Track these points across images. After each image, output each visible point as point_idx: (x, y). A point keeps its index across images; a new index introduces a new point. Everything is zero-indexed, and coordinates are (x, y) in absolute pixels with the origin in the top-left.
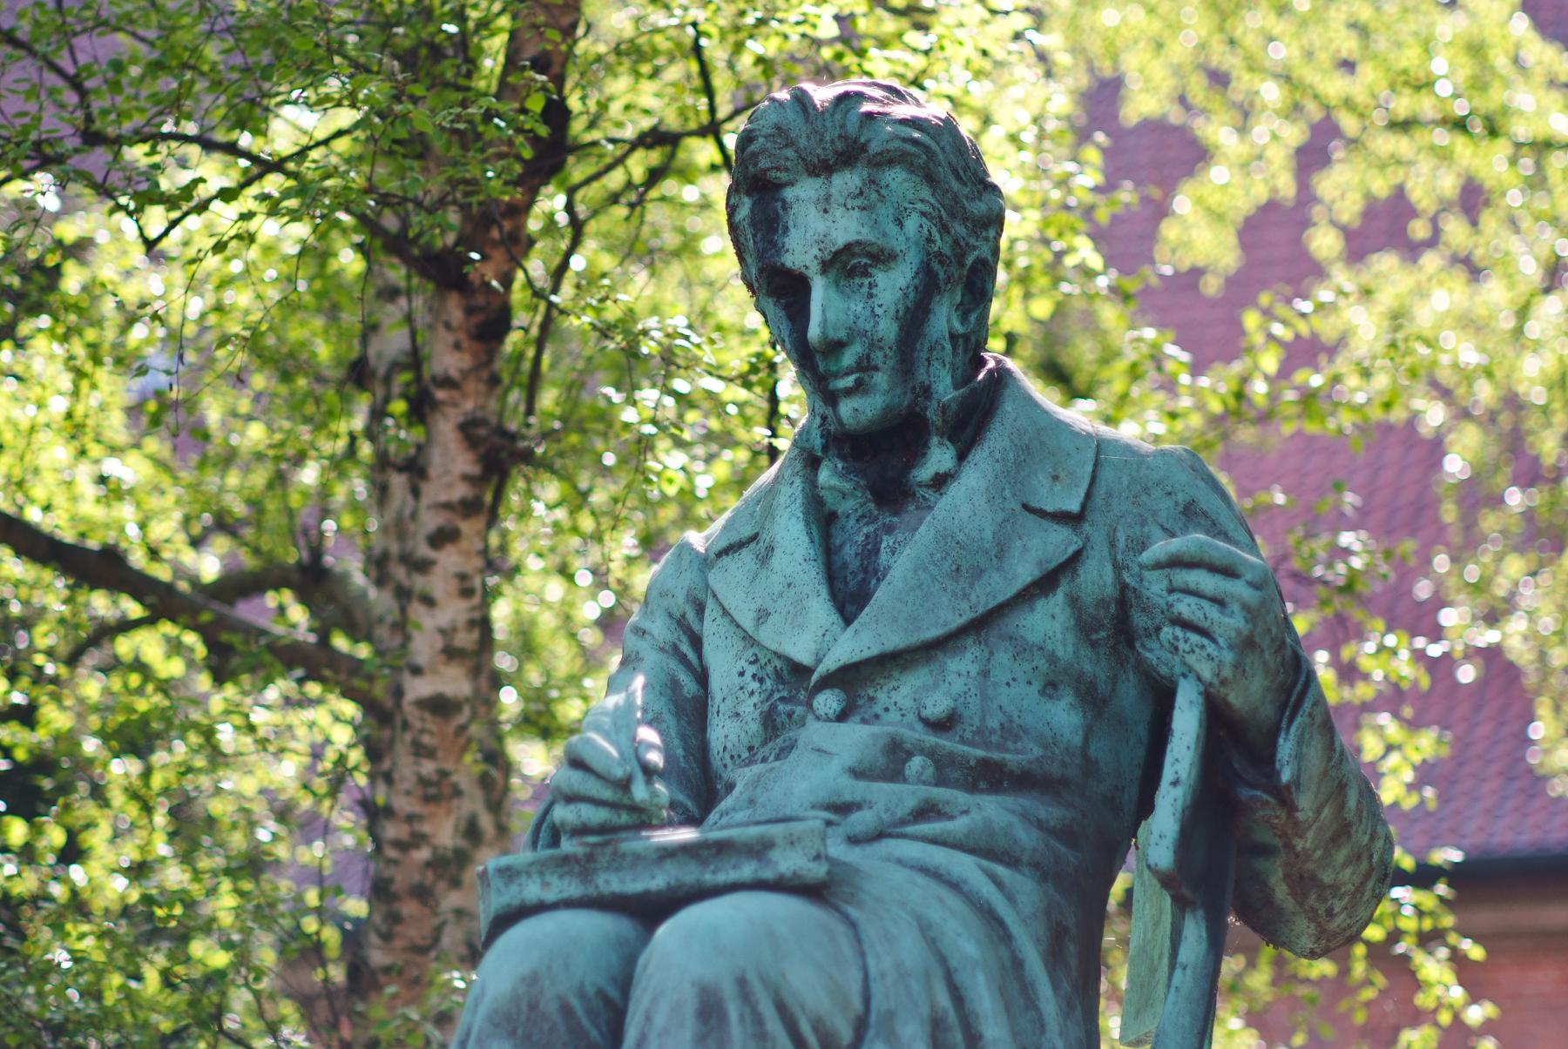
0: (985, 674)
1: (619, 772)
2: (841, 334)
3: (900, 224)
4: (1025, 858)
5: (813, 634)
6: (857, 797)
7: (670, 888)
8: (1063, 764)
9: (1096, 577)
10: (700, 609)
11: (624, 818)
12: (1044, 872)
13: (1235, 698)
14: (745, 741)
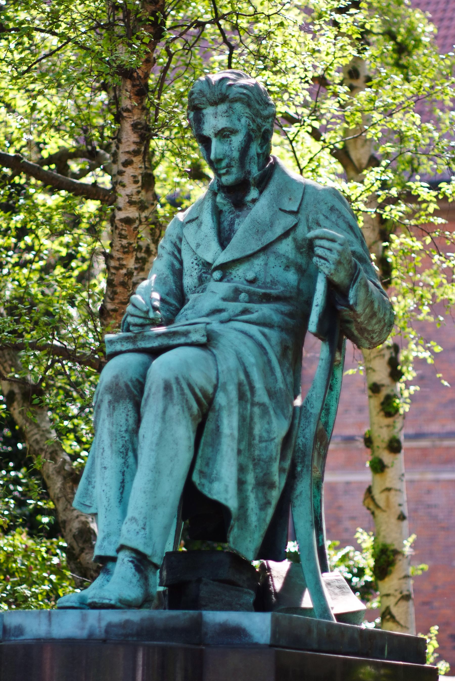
0: (266, 264)
1: (145, 309)
2: (221, 157)
3: (239, 120)
4: (276, 325)
5: (213, 253)
6: (223, 307)
7: (160, 346)
8: (291, 292)
10: (181, 240)
12: (282, 328)
13: (335, 279)
14: (194, 285)
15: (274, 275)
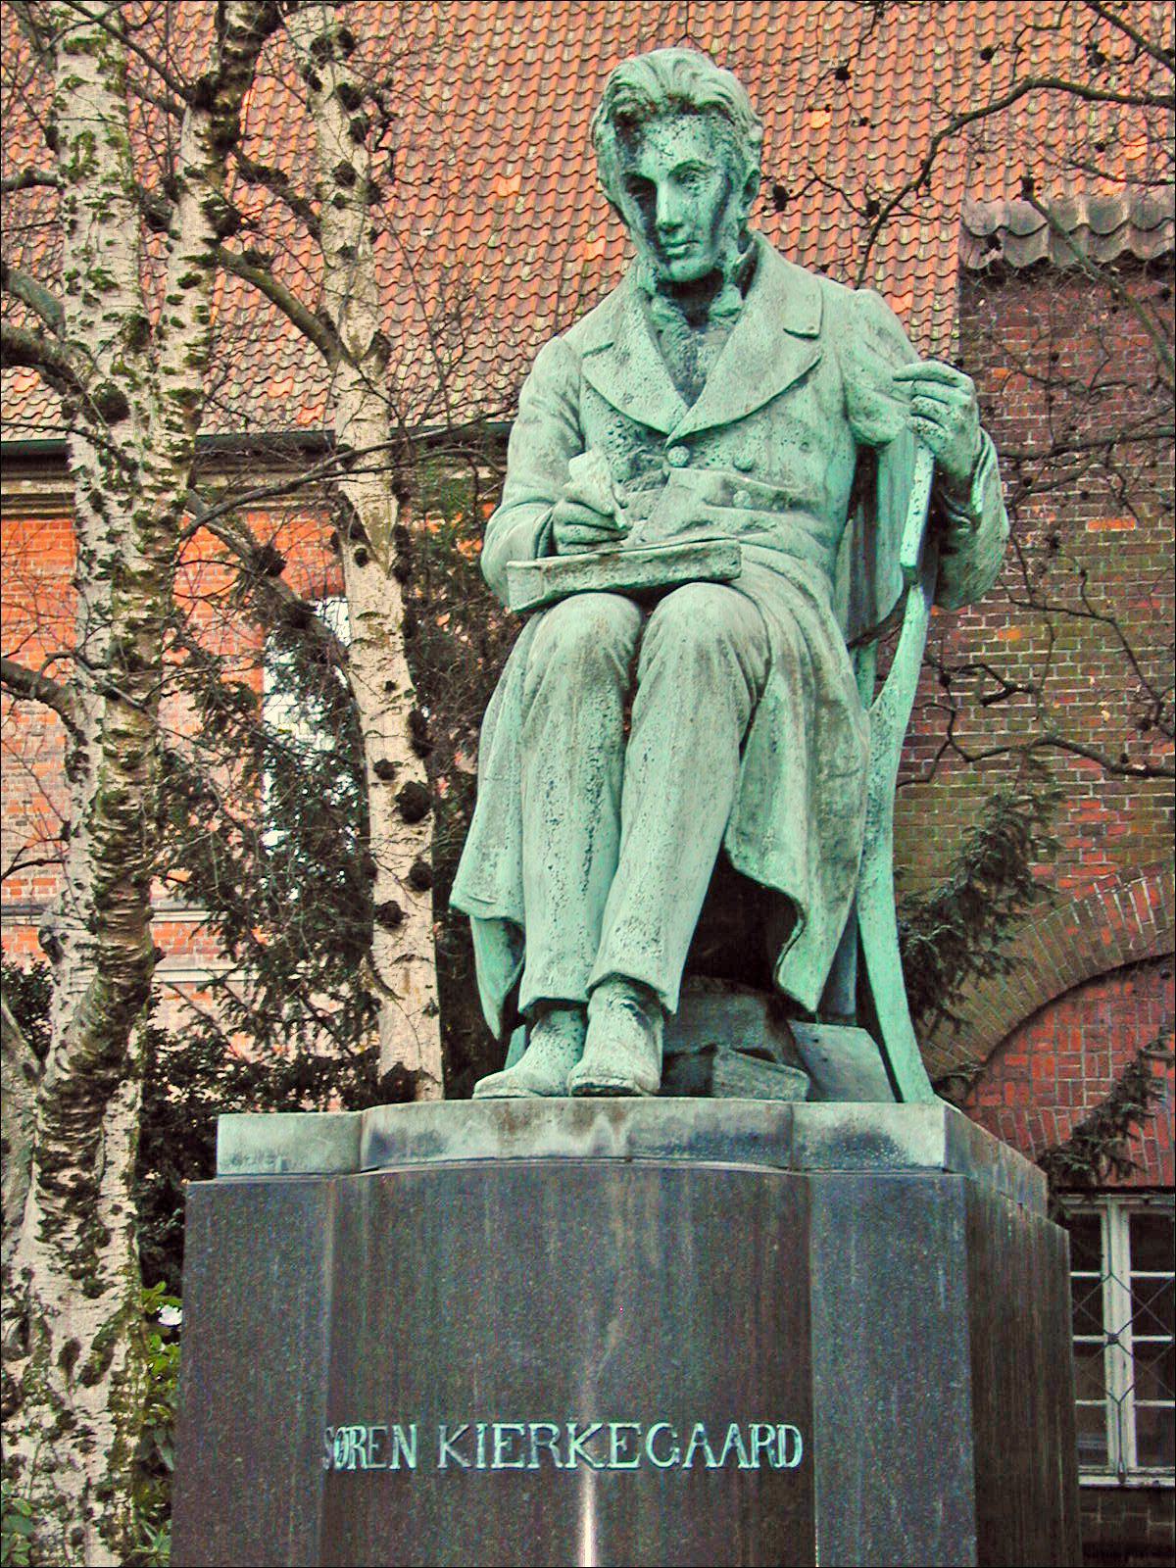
1: (609, 509)
2: (677, 220)
11: (605, 535)
15: (785, 459)
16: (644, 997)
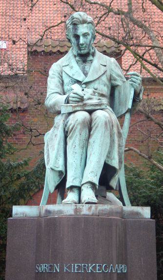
2: (84, 43)
9: (108, 73)
16: (93, 185)
